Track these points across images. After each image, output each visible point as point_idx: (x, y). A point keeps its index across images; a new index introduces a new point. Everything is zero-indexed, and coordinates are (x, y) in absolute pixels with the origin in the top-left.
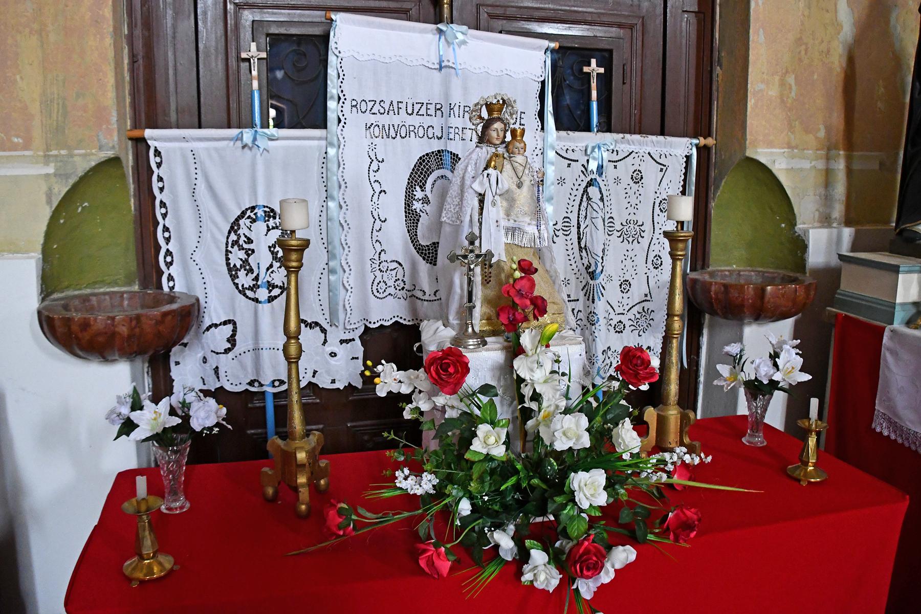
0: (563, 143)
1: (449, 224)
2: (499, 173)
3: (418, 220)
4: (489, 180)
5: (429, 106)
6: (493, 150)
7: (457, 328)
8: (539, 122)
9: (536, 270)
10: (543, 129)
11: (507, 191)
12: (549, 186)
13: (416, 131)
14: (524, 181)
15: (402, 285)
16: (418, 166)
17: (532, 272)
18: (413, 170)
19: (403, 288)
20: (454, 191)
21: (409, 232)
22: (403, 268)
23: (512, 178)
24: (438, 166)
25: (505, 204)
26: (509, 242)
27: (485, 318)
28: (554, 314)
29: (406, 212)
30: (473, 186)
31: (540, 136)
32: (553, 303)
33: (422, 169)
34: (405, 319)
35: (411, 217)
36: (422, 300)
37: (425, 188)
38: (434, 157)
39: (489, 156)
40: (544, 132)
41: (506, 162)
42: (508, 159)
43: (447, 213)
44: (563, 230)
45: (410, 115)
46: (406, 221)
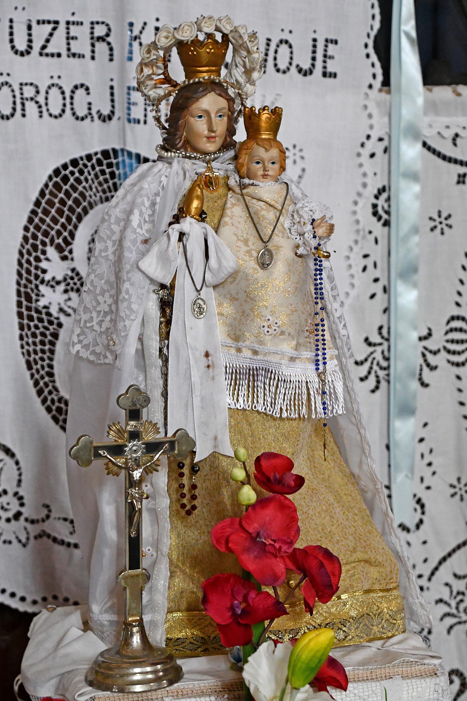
0: (446, 120)
1: (91, 362)
2: (211, 232)
3: (56, 336)
4: (185, 247)
5: (74, 30)
6: (201, 167)
7: (110, 632)
8: (378, 64)
9: (300, 481)
10: (386, 82)
11: (234, 275)
12: (406, 238)
13: (41, 99)
14: (278, 248)
15: (15, 507)
16: (51, 193)
17: (289, 486)
18: (38, 203)
19: (17, 516)
20: (100, 277)
21: (29, 367)
22: (17, 463)
23: (246, 242)
24: (104, 192)
25: (228, 309)
26: (241, 405)
27: (184, 606)
28: (368, 591)
29: (20, 315)
30: (144, 265)
31: (378, 104)
32: (366, 561)
33: (62, 202)
34: (23, 599)
35: (36, 327)
36: (69, 545)
37: (71, 252)
38: (93, 168)
39: (188, 184)
40: (389, 92)
41: (231, 199)
42: (237, 190)
43: (83, 333)
44: (449, 352)
45: (22, 54)
46: (21, 338)
